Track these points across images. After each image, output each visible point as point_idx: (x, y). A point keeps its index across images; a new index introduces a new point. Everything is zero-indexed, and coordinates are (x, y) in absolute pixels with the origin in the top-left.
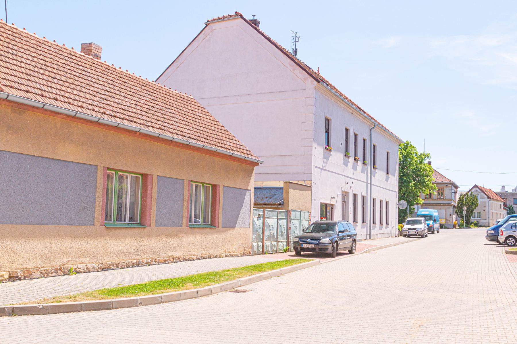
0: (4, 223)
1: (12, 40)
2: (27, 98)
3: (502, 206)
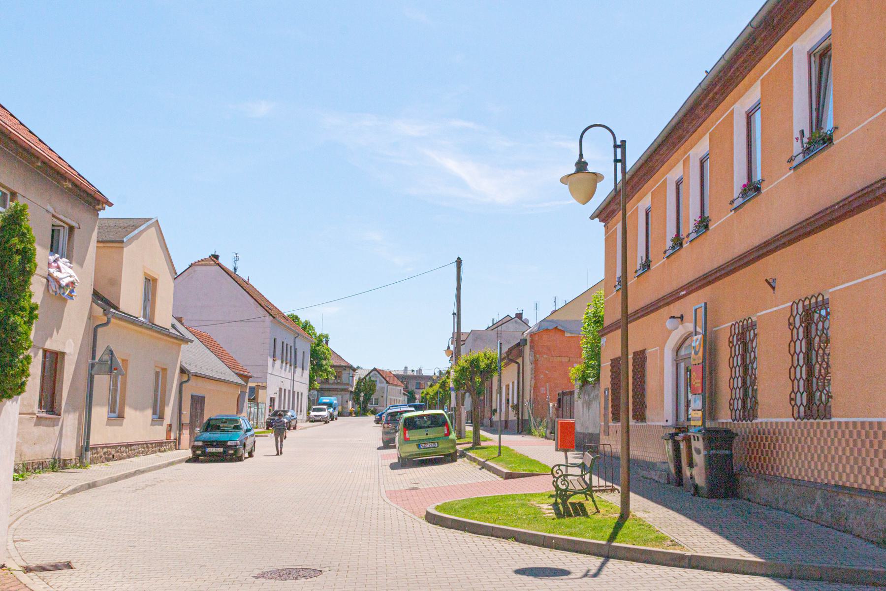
3: (402, 391)
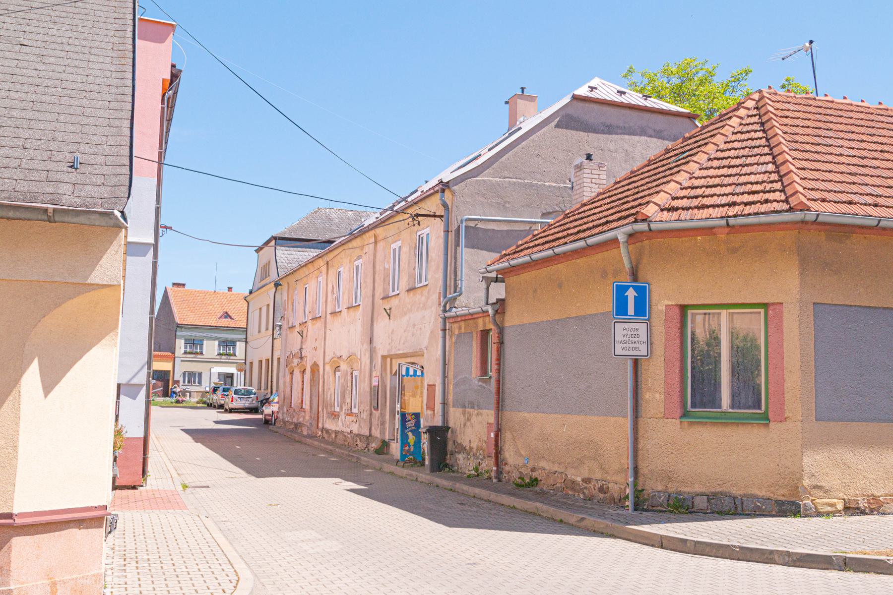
0: (829, 420)
1: (825, 122)
2: (849, 214)
